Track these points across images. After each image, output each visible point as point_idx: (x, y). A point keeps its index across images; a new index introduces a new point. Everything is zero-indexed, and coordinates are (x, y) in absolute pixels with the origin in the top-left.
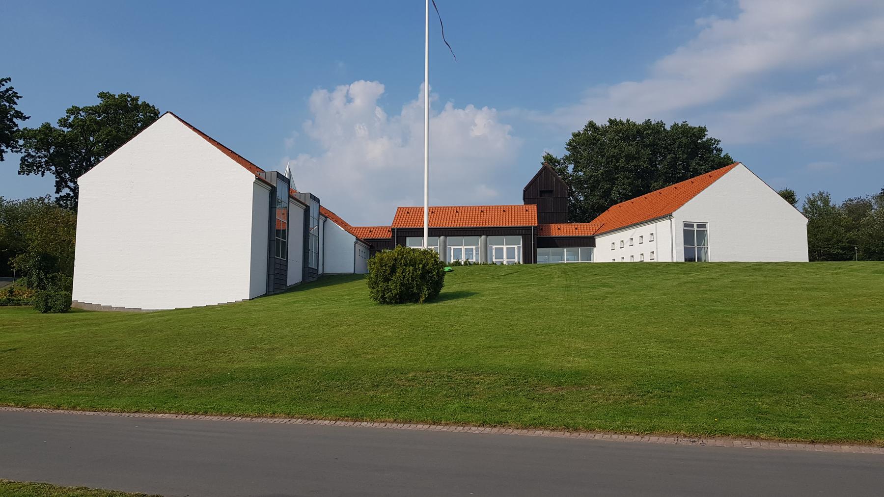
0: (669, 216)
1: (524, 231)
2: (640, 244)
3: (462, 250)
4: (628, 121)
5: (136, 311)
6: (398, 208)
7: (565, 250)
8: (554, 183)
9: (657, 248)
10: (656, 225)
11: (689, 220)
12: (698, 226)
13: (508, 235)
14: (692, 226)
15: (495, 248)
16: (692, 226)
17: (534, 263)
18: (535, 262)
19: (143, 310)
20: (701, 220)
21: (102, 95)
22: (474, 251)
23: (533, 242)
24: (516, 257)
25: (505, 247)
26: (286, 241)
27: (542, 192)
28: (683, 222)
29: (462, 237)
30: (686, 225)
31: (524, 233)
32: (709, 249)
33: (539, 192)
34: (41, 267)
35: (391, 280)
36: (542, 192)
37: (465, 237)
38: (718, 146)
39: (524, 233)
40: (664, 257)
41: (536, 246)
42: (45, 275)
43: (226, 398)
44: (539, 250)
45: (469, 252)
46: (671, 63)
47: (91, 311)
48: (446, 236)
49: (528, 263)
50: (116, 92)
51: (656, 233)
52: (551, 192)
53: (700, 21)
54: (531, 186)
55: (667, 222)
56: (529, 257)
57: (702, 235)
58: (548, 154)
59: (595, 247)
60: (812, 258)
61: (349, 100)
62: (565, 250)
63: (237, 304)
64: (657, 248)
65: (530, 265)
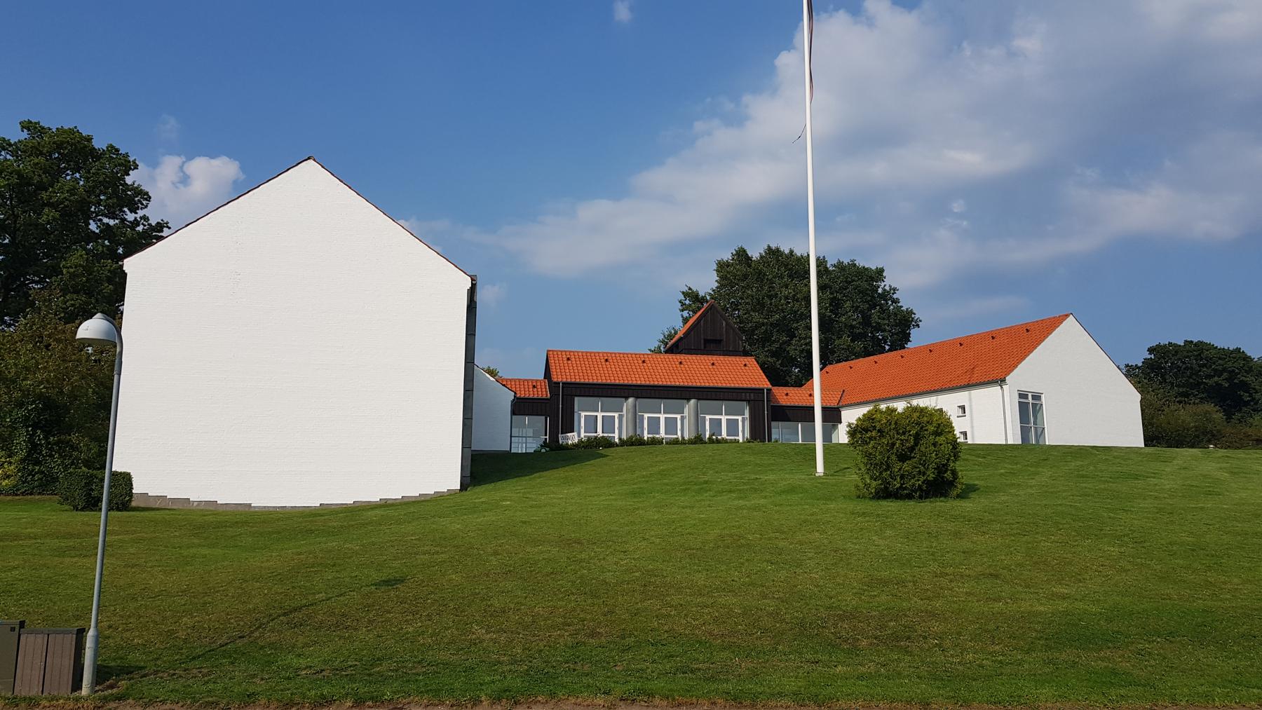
0: (1001, 381)
1: (752, 395)
2: (958, 417)
3: (598, 419)
4: (791, 252)
5: (240, 508)
6: (548, 351)
7: (800, 425)
8: (724, 329)
9: (972, 427)
10: (970, 395)
13: (644, 398)
15: (648, 417)
17: (768, 441)
18: (770, 440)
19: (254, 507)
21: (27, 126)
22: (740, 423)
23: (766, 412)
24: (617, 431)
25: (662, 417)
27: (706, 341)
29: (660, 400)
32: (1046, 429)
33: (702, 341)
34: (40, 422)
35: (910, 458)
36: (706, 341)
37: (664, 400)
38: (895, 296)
39: (752, 398)
41: (770, 419)
42: (46, 438)
44: (773, 424)
45: (671, 425)
46: (659, 178)
47: (158, 509)
48: (637, 398)
50: (53, 121)
51: (971, 406)
52: (720, 341)
53: (699, 126)
54: (692, 333)
55: (995, 390)
56: (759, 432)
57: (1037, 408)
58: (690, 289)
59: (841, 422)
60: (1149, 440)
61: (185, 180)
62: (800, 425)
63: (438, 498)
64: (972, 427)
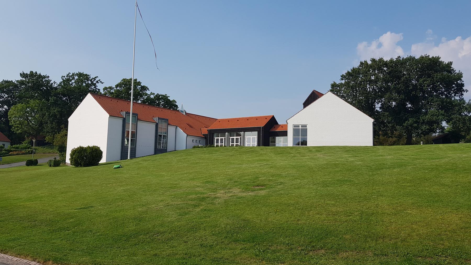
11: (296, 123)
12: (302, 126)
14: (299, 126)
16: (299, 126)
20: (304, 123)
26: (166, 135)
28: (293, 125)
30: (295, 126)
31: (258, 130)
40: (256, 137)
43: (281, 204)
49: (260, 146)
65: (260, 147)
